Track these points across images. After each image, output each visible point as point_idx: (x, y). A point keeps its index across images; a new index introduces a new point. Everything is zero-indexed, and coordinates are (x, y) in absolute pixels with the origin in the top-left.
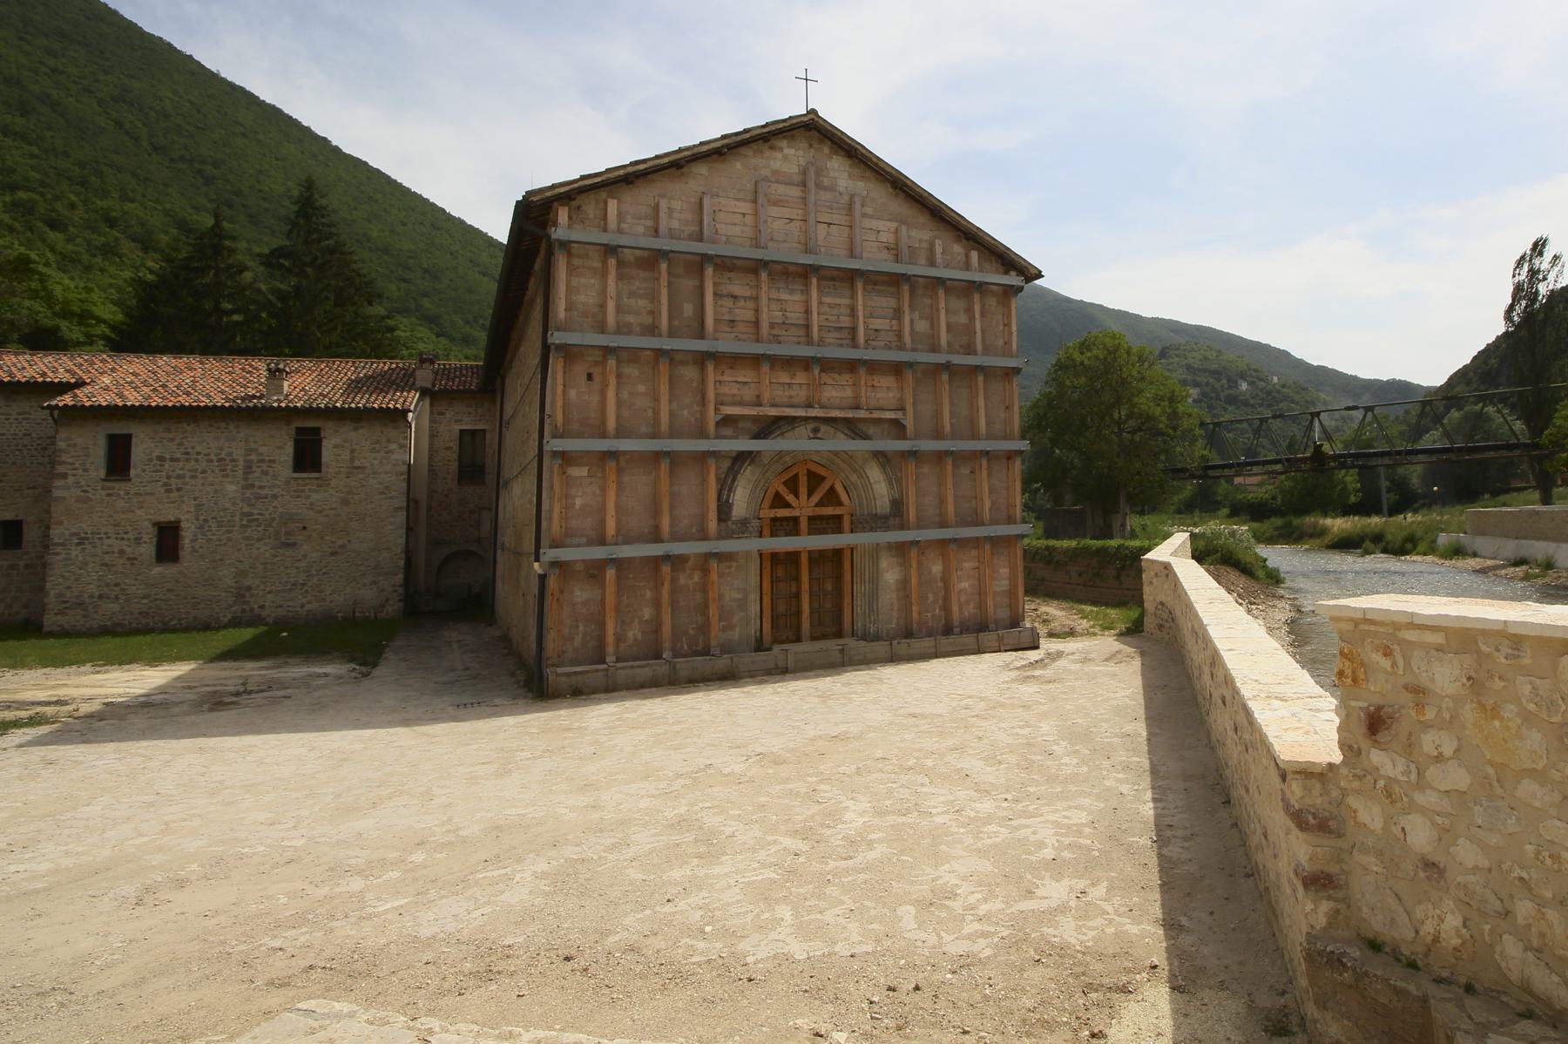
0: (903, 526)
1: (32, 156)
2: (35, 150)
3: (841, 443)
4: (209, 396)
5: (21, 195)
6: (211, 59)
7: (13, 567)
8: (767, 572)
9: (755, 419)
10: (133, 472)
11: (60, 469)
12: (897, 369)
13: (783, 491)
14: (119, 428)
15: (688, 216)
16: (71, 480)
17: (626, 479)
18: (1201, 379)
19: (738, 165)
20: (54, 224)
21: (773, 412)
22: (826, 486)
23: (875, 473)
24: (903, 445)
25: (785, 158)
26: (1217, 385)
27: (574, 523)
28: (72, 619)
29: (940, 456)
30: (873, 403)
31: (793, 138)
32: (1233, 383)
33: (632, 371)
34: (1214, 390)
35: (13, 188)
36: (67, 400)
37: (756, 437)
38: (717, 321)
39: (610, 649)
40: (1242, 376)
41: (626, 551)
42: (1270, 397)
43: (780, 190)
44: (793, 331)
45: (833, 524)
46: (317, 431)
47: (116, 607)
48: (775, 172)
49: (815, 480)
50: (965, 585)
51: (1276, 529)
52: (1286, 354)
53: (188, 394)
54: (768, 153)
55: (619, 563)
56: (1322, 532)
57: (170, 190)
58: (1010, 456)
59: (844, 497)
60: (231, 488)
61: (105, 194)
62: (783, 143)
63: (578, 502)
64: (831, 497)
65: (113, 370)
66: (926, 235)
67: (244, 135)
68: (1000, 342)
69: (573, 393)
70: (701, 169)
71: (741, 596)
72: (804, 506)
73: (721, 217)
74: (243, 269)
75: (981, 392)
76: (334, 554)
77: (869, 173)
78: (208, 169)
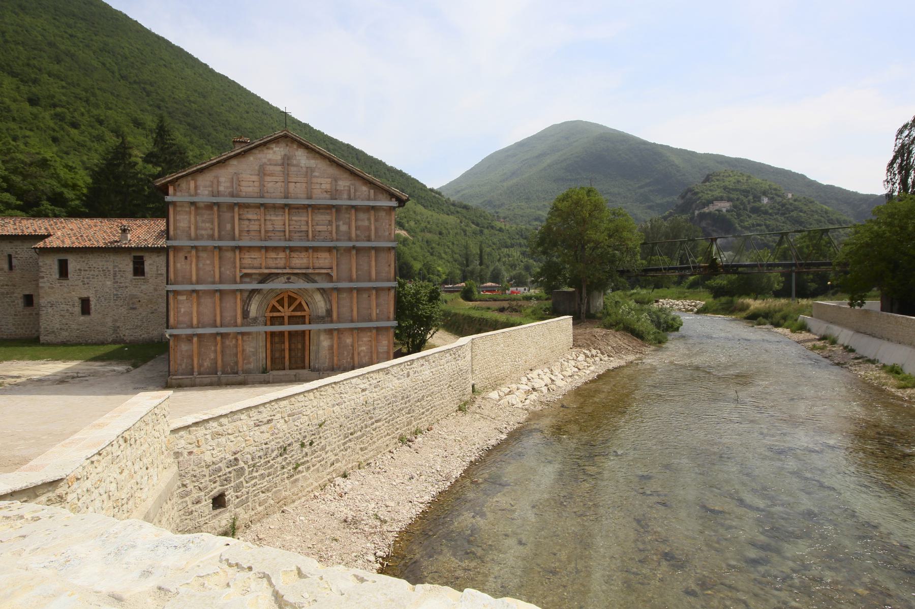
0: (332, 322)
1: (63, 87)
2: (64, 83)
3: (301, 284)
4: (98, 241)
5: (58, 110)
6: (147, 22)
7: (31, 314)
8: (269, 340)
9: (260, 274)
10: (69, 276)
11: (42, 275)
12: (329, 250)
13: (277, 305)
14: (63, 257)
15: (228, 184)
16: (46, 279)
17: (202, 301)
18: (734, 196)
19: (251, 158)
20: (75, 125)
21: (267, 271)
22: (297, 303)
23: (318, 297)
24: (330, 285)
25: (274, 152)
26: (745, 200)
27: (181, 319)
28: (50, 338)
29: (351, 290)
30: (317, 265)
31: (278, 142)
32: (757, 198)
33: (203, 255)
34: (742, 203)
35: (55, 106)
36: (41, 244)
37: (260, 282)
38: (240, 231)
39: (196, 370)
40: (765, 193)
41: (200, 331)
42: (784, 209)
43: (271, 168)
44: (278, 234)
45: (301, 320)
46: (142, 258)
47: (67, 334)
48: (269, 160)
49: (292, 300)
50: (364, 348)
51: (722, 304)
52: (803, 177)
53: (90, 240)
54: (266, 151)
55: (199, 336)
56: (744, 308)
57: (130, 101)
58: (389, 289)
59: (306, 307)
60: (109, 283)
61: (97, 106)
62: (273, 146)
63: (182, 310)
64: (300, 307)
65: (64, 227)
66: (347, 183)
67: (165, 66)
68: (387, 233)
69: (179, 265)
70: (234, 162)
71: (255, 350)
72: (286, 312)
73: (243, 183)
74: (136, 164)
75: (373, 259)
76: (152, 313)
77: (317, 156)
78: (148, 87)
